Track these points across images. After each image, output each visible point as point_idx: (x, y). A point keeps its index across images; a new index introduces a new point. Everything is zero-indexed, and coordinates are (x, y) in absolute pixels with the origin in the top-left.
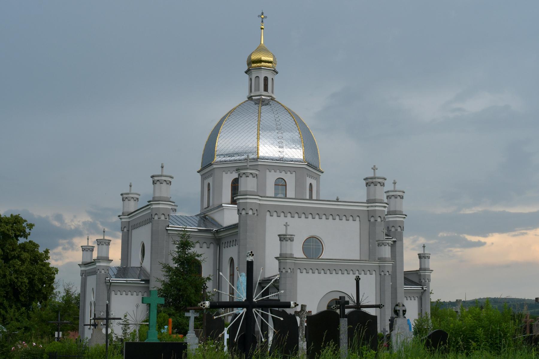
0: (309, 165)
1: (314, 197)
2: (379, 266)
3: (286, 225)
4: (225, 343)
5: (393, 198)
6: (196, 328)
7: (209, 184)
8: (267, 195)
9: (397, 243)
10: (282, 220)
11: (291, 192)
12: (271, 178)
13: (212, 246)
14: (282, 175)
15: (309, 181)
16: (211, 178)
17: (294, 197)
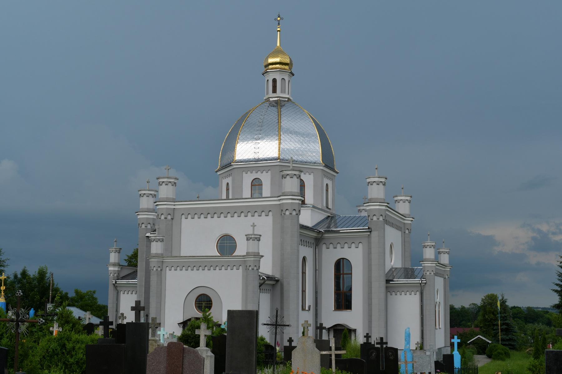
0: (326, 166)
2: (245, 261)
3: (254, 226)
6: (458, 348)
7: (228, 184)
8: (243, 197)
10: (250, 220)
11: (266, 191)
12: (248, 179)
14: (258, 175)
15: (326, 181)
16: (231, 178)
17: (269, 196)
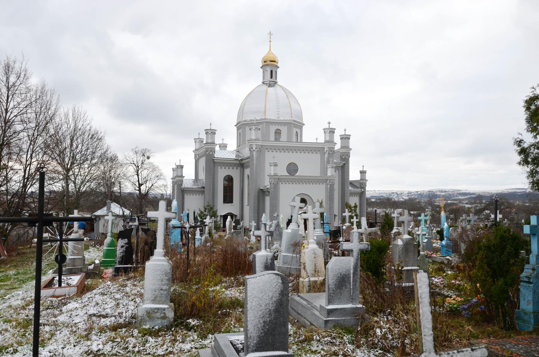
1: (299, 141)
4: (255, 159)
12: (273, 129)
13: (239, 168)
14: (279, 127)
15: (295, 130)
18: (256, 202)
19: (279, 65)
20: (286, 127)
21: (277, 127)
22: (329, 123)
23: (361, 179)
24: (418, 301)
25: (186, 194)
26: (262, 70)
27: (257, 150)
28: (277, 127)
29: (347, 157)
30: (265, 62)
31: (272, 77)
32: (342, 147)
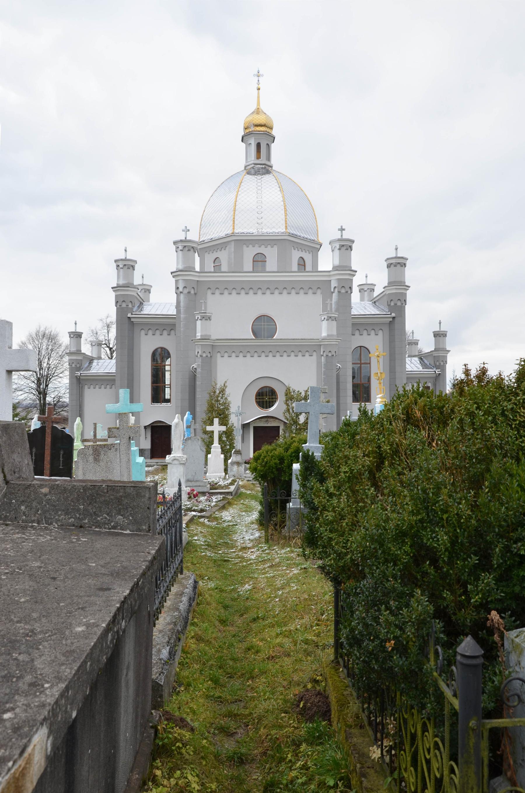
5: (392, 266)
9: (396, 319)
12: (249, 253)
14: (262, 250)
15: (296, 255)
18: (187, 396)
19: (274, 132)
20: (276, 248)
21: (258, 250)
22: (342, 230)
23: (436, 350)
24: (337, 630)
25: (86, 387)
26: (243, 145)
27: (186, 291)
28: (258, 250)
29: (399, 303)
30: (246, 129)
31: (258, 157)
32: (391, 284)
